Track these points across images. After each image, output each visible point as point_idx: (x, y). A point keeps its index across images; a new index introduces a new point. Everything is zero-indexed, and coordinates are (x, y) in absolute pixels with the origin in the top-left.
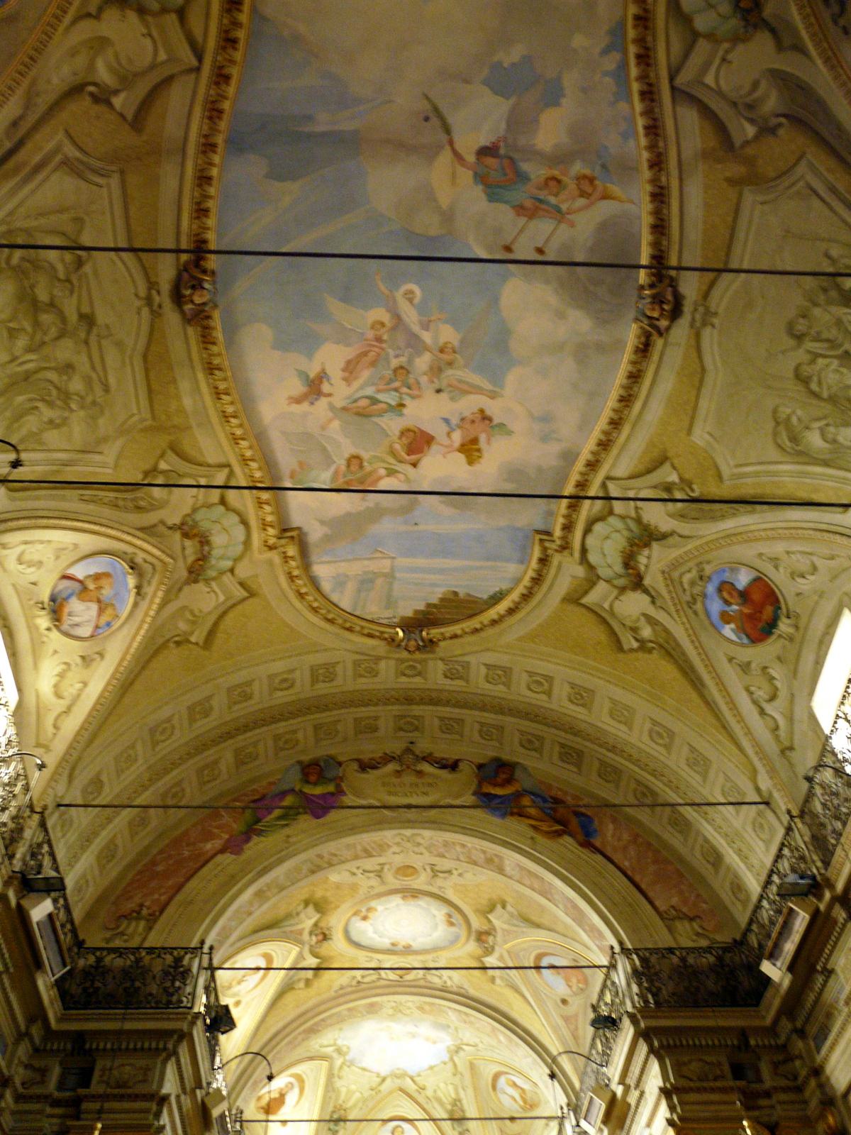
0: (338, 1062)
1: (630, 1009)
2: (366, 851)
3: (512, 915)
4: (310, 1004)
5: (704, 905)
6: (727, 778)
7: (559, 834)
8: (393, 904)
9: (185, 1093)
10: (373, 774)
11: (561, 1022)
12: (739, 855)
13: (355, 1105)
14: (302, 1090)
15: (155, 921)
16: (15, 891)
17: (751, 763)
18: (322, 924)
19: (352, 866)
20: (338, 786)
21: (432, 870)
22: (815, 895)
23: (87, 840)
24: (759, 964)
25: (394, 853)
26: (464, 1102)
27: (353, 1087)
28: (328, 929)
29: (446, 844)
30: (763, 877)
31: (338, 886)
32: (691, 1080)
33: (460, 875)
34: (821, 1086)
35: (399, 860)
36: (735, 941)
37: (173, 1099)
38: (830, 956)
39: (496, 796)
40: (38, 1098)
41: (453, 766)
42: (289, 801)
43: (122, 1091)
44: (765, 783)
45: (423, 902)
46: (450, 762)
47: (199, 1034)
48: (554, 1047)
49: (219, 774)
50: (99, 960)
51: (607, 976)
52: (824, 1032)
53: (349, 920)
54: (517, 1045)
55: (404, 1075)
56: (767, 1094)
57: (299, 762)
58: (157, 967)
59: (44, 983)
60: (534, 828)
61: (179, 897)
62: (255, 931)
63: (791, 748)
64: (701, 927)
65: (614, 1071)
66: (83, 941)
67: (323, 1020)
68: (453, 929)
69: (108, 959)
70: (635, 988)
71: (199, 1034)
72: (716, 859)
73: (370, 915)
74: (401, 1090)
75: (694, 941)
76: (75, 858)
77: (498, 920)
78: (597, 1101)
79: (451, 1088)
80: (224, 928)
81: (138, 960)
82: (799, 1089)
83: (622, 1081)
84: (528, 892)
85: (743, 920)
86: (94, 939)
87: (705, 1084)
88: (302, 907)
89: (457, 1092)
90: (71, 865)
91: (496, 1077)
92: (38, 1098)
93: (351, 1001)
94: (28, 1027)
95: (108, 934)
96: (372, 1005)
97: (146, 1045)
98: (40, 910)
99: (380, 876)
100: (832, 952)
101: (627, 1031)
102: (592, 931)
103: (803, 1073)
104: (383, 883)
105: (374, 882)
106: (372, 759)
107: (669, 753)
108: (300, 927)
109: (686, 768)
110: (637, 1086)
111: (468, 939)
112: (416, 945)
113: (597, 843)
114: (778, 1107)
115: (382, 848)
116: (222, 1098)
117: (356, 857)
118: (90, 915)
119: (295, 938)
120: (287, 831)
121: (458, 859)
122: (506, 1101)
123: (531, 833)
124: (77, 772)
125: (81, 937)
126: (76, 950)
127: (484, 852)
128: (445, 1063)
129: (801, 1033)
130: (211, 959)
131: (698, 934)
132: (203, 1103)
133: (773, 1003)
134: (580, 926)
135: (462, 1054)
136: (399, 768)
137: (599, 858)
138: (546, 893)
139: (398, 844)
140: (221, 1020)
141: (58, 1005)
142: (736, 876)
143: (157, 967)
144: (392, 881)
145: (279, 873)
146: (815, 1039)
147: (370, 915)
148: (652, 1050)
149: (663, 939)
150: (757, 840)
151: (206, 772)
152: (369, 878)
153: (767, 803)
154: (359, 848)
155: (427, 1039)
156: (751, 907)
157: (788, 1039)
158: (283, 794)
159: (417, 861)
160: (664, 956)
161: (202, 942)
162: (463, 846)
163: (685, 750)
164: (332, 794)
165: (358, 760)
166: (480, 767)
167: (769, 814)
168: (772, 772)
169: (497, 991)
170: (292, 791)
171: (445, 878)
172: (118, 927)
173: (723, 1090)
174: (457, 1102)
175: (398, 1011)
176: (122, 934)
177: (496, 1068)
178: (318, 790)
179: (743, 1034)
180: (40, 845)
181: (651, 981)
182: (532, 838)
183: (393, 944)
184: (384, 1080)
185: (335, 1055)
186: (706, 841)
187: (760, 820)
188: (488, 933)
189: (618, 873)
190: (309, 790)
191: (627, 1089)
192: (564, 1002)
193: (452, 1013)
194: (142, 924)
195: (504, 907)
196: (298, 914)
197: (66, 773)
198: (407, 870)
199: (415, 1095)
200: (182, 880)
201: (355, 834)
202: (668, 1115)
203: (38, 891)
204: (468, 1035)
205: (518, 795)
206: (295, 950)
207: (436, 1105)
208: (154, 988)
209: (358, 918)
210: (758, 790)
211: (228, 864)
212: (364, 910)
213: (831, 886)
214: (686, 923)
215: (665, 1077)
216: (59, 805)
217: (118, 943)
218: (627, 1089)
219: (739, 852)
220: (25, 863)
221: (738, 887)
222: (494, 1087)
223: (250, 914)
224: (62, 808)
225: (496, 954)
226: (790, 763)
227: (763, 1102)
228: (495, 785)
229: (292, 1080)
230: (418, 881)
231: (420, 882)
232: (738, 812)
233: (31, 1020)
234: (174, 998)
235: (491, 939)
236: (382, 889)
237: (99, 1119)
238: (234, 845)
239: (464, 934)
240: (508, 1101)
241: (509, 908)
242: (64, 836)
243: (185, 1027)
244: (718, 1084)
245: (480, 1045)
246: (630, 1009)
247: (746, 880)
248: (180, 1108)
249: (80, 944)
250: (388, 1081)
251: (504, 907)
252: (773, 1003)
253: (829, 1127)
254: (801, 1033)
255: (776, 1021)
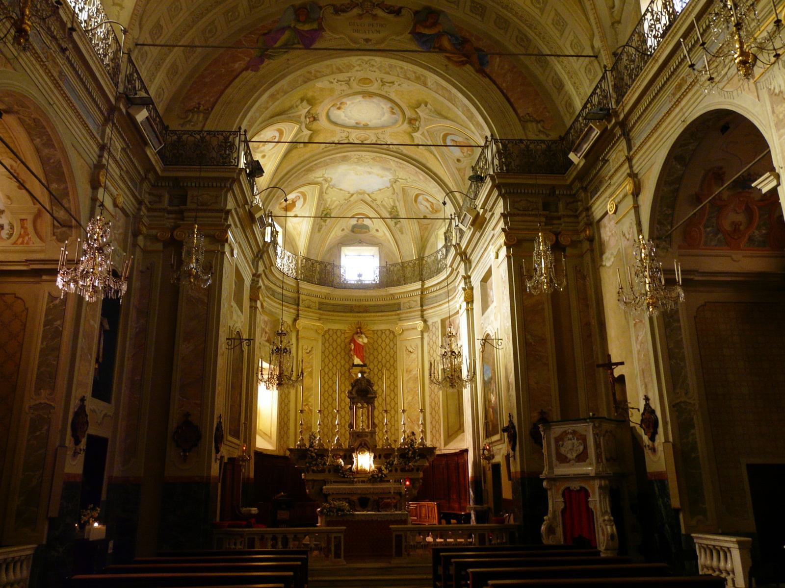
0: (325, 186)
1: (491, 173)
2: (339, 69)
3: (431, 111)
4: (306, 156)
5: (548, 114)
6: (576, 37)
7: (463, 63)
8: (358, 100)
9: (239, 207)
10: (343, 16)
11: (456, 172)
12: (574, 86)
13: (336, 207)
14: (305, 199)
15: (209, 114)
16: (123, 105)
17: (592, 30)
18: (312, 112)
19: (331, 78)
20: (320, 24)
21: (381, 81)
22: (607, 120)
23: (158, 65)
24: (568, 154)
25: (357, 71)
26: (398, 208)
27: (334, 199)
28: (317, 114)
29: (391, 66)
30: (584, 102)
31: (322, 90)
32: (519, 210)
33: (399, 85)
34: (588, 216)
35: (361, 75)
36: (560, 137)
37: (233, 211)
38: (608, 153)
39: (425, 35)
40: (160, 210)
41: (397, 12)
42: (287, 35)
43: (205, 207)
44: (597, 44)
45: (376, 100)
46: (396, 8)
47: (243, 178)
48: (453, 186)
49: (239, 15)
50: (179, 138)
51: (483, 153)
52: (596, 190)
53: (329, 109)
54: (430, 181)
55: (364, 193)
56: (559, 218)
57: (293, 6)
58: (215, 142)
59: (151, 153)
60: (448, 58)
61: (223, 98)
62: (271, 117)
63: (619, 22)
64: (543, 127)
65: (479, 202)
66: (168, 126)
67: (316, 164)
68: (394, 116)
69: (184, 137)
70: (496, 162)
71: (243, 178)
72: (560, 86)
73: (342, 107)
74: (362, 200)
75: (537, 135)
76: (153, 76)
77: (422, 112)
78: (469, 216)
79: (391, 200)
80: (252, 118)
81: (203, 138)
82: (577, 217)
83: (483, 207)
84: (441, 99)
85: (568, 124)
86: (174, 125)
87: (527, 213)
88: (299, 101)
89: (394, 203)
90: (151, 81)
91: (417, 196)
92: (160, 210)
93: (332, 154)
94: (146, 175)
95: (182, 121)
96: (345, 157)
97: (214, 184)
98: (142, 116)
99: (349, 84)
100: (609, 151)
101: (488, 184)
102: (477, 125)
103: (581, 209)
104: (350, 88)
105: (345, 87)
106: (343, 5)
107: (542, 14)
108: (299, 113)
109: (552, 26)
110: (490, 211)
111: (403, 123)
112: (371, 124)
113: (488, 71)
114: (563, 225)
115: (350, 67)
116: (260, 209)
117: (333, 73)
118: (168, 109)
119: (297, 120)
120: (286, 56)
121: (398, 76)
122: (422, 208)
123: (446, 62)
124: (144, 20)
125: (166, 124)
126: (164, 132)
127: (415, 73)
128: (388, 188)
129: (585, 189)
130: (246, 138)
131: (540, 131)
132: (250, 211)
133: (572, 174)
134: (471, 121)
135: (398, 183)
136: (360, 12)
137: (487, 80)
138: (452, 100)
139: (359, 65)
140: (256, 169)
141: (161, 163)
142: (570, 98)
143: (215, 142)
144: (356, 87)
145: (284, 83)
146: (591, 192)
147: (342, 107)
148: (500, 194)
149: (518, 133)
150: (586, 78)
151: (230, 14)
152: (341, 85)
153: (596, 57)
154: (334, 67)
155: (378, 175)
156: (575, 117)
157: (577, 191)
158: (283, 30)
159: (371, 76)
160: (516, 144)
161: (240, 128)
162: (402, 68)
163: (553, 14)
164: (315, 30)
165: (333, 5)
166: (416, 13)
167: (596, 64)
168: (603, 37)
169: (420, 154)
170: (289, 27)
171: (390, 87)
172: (187, 117)
173: (536, 216)
174: (394, 207)
175: (360, 161)
176: (190, 121)
177: (417, 192)
178: (306, 27)
179: (553, 188)
180: (131, 75)
181: (506, 158)
182: (446, 66)
183: (357, 123)
184: (352, 195)
185: (323, 182)
186: (556, 74)
187: (590, 66)
188: (416, 120)
189: (499, 91)
190: (300, 27)
191: (485, 211)
192: (458, 160)
193: (393, 162)
194: (202, 115)
195: (426, 106)
196: (297, 106)
197: (137, 24)
198: (365, 81)
199: (371, 203)
200: (222, 88)
201: (331, 58)
202: (503, 227)
203: (137, 104)
204: (402, 174)
205: (439, 35)
206: (297, 127)
207: (382, 208)
208: (214, 154)
209: (335, 108)
210: (593, 47)
211: (251, 78)
212: (339, 103)
213: (617, 116)
214: (534, 124)
215: (505, 208)
216: (137, 45)
217: (188, 127)
218: (485, 211)
219: (574, 84)
220: (125, 87)
221: (569, 104)
222: (416, 201)
223: (267, 109)
224: (139, 47)
225: (420, 132)
226: (615, 32)
227: (555, 222)
228: (426, 27)
229: (299, 194)
230: (372, 87)
231: (374, 88)
232: (577, 60)
233: (147, 171)
234: (227, 160)
235: (417, 123)
236: (350, 91)
237: (196, 223)
238: (254, 65)
239: (401, 120)
240: (423, 207)
241: (429, 106)
242: (144, 63)
243: (235, 176)
244: (533, 212)
245: (409, 180)
246: (491, 173)
247: (575, 103)
248: (237, 214)
249: (166, 128)
250: (355, 195)
251: (426, 106)
252: (572, 174)
253: (586, 235)
254: (585, 189)
255: (572, 183)
